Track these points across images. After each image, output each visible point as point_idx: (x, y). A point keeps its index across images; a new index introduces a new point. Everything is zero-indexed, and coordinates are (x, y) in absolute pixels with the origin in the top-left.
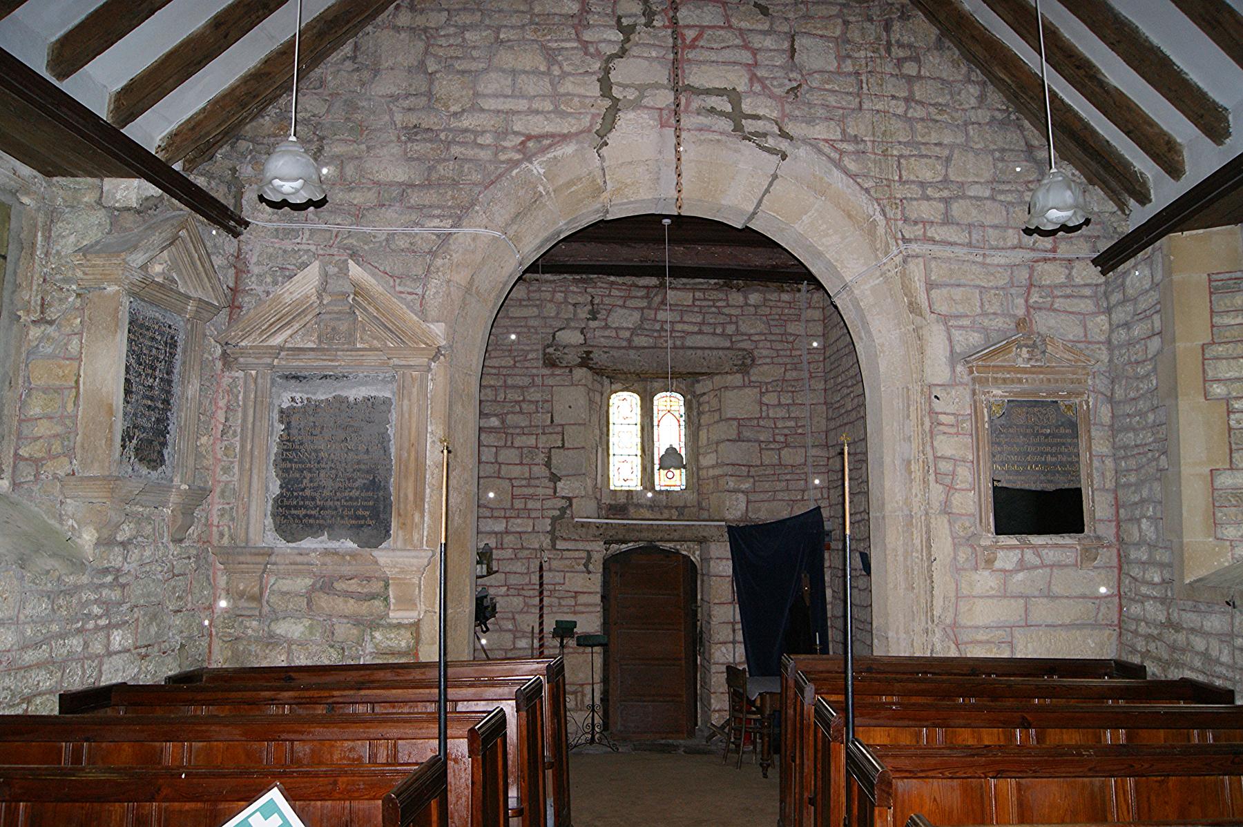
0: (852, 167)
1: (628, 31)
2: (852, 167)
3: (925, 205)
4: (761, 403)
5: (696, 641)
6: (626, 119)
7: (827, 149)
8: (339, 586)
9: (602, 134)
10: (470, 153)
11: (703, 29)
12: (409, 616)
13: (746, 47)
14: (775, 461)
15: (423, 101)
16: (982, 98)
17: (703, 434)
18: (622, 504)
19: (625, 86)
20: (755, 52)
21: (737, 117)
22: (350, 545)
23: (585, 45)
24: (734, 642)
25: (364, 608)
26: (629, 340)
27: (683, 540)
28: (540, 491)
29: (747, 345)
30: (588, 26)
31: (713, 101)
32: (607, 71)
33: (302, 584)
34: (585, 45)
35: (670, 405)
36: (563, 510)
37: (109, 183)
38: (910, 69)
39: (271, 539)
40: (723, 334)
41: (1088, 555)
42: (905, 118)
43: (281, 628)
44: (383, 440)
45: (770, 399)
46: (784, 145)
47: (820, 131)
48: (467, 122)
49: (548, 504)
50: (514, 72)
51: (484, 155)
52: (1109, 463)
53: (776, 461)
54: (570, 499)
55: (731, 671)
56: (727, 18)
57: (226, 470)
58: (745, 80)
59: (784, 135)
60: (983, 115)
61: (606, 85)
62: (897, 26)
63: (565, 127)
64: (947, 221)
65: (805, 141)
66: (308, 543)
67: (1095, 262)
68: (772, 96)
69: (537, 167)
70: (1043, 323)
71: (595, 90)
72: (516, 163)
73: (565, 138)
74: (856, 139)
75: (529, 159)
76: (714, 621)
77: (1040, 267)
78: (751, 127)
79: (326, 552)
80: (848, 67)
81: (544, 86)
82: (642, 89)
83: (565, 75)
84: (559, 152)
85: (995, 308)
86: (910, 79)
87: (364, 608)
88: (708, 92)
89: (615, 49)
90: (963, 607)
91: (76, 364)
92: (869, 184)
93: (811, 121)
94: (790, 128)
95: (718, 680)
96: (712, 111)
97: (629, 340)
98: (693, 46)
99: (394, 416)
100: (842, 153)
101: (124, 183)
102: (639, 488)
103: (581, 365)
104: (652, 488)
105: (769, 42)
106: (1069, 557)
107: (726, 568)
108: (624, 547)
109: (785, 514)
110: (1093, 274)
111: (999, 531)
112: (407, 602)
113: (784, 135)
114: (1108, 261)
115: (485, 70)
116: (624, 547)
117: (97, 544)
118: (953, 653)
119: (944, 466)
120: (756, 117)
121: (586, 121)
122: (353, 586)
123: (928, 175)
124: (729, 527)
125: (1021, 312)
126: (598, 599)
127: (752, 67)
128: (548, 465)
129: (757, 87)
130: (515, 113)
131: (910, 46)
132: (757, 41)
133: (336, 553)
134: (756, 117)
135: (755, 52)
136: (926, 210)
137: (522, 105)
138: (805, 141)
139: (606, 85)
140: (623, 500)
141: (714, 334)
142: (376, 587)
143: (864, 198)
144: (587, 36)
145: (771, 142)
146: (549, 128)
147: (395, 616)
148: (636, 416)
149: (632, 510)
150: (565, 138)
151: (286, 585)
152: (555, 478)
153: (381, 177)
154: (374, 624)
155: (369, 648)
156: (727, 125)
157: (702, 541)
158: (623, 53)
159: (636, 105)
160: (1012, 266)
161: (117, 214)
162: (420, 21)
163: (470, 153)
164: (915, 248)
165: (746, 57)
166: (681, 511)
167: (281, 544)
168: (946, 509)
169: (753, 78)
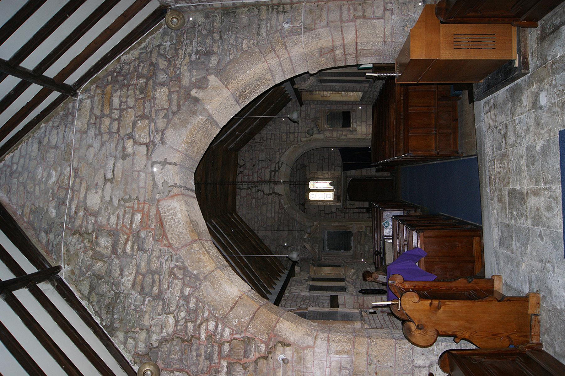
0: (284, 150)
1: (259, 190)
2: (284, 150)
3: (291, 137)
4: (313, 163)
5: (370, 179)
6: (276, 191)
7: (281, 155)
8: (359, 240)
9: (279, 195)
10: (282, 218)
11: (258, 177)
12: (364, 227)
13: (261, 169)
14: (327, 159)
15: (272, 227)
16: (270, 126)
17: (320, 177)
18: (337, 196)
19: (270, 191)
20: (262, 167)
21: (275, 171)
22: (352, 238)
23: (261, 198)
24: (371, 170)
25: (363, 236)
26: (298, 194)
27: (346, 182)
28: (335, 216)
29: (299, 166)
30: (258, 198)
31: (272, 175)
32: (267, 194)
33: (359, 246)
34: (261, 198)
35: (312, 185)
36: (339, 210)
37: (296, 272)
38: (265, 139)
39: (351, 251)
40: (296, 172)
41: (354, 111)
42: (274, 140)
43: (367, 250)
44: (334, 232)
45: (312, 160)
46: (281, 163)
47: (278, 156)
48: (276, 219)
49: (338, 214)
50: (267, 211)
51: (283, 216)
52: (338, 106)
53: (327, 159)
54: (337, 209)
55: (377, 171)
56: (256, 172)
57: (339, 260)
58: (267, 169)
59: (279, 162)
60: (273, 125)
61: (269, 194)
62: (256, 141)
63: (278, 202)
64: (294, 133)
65: (280, 159)
66: (352, 245)
67: (301, 106)
68: (271, 165)
69: (286, 206)
70: (312, 116)
71: (270, 196)
72: (285, 210)
73: (280, 201)
74: (279, 149)
75: (284, 208)
76: (366, 175)
77: (302, 116)
78: (277, 169)
79: (354, 242)
80: (265, 150)
81: (269, 205)
82: (270, 188)
83: (267, 202)
84: (283, 203)
85: (310, 125)
86: (267, 139)
87: (363, 236)
88: (271, 176)
89: (262, 193)
90: (363, 133)
91: (411, 89)
92: (287, 147)
93: (276, 157)
94: (277, 161)
95: (380, 174)
96: (274, 175)
97: (298, 194)
98: (262, 179)
99: (330, 231)
100: (281, 152)
101: (296, 269)
102: (333, 193)
103: (304, 206)
104: (333, 189)
105: (260, 165)
106: (354, 113)
107: (353, 172)
108: (348, 196)
109: (340, 157)
110: (303, 107)
111: (350, 127)
112: (362, 228)
113: (279, 162)
114: (301, 104)
115: (266, 216)
116: (348, 196)
117: (354, 269)
118: (371, 135)
119: (338, 136)
120: (275, 167)
121: (277, 198)
122: (359, 238)
123: (285, 137)
124: (344, 171)
125: (310, 120)
126: (361, 202)
127: (266, 168)
128: (328, 214)
129: (269, 167)
130: (275, 210)
131: (260, 139)
132: (260, 167)
133: (354, 240)
134: (275, 167)
135: (262, 167)
136: (292, 137)
137: (273, 209)
138: (280, 159)
139: (269, 194)
140: (336, 197)
141: (296, 174)
142: (359, 233)
143: (290, 149)
144: (260, 198)
145: (280, 165)
146: (278, 205)
147: (364, 230)
148: (315, 193)
149: (338, 194)
150: (280, 201)
151: (359, 249)
152: (332, 212)
153: (287, 234)
154: (365, 234)
155: (370, 235)
156: (277, 173)
157: (346, 177)
158: (263, 191)
159: (274, 189)
160: (302, 122)
161: (301, 270)
162: (256, 228)
163: (282, 218)
164: (299, 140)
165: (263, 169)
166: (339, 182)
167: (352, 250)
168: (346, 136)
169: (268, 168)
